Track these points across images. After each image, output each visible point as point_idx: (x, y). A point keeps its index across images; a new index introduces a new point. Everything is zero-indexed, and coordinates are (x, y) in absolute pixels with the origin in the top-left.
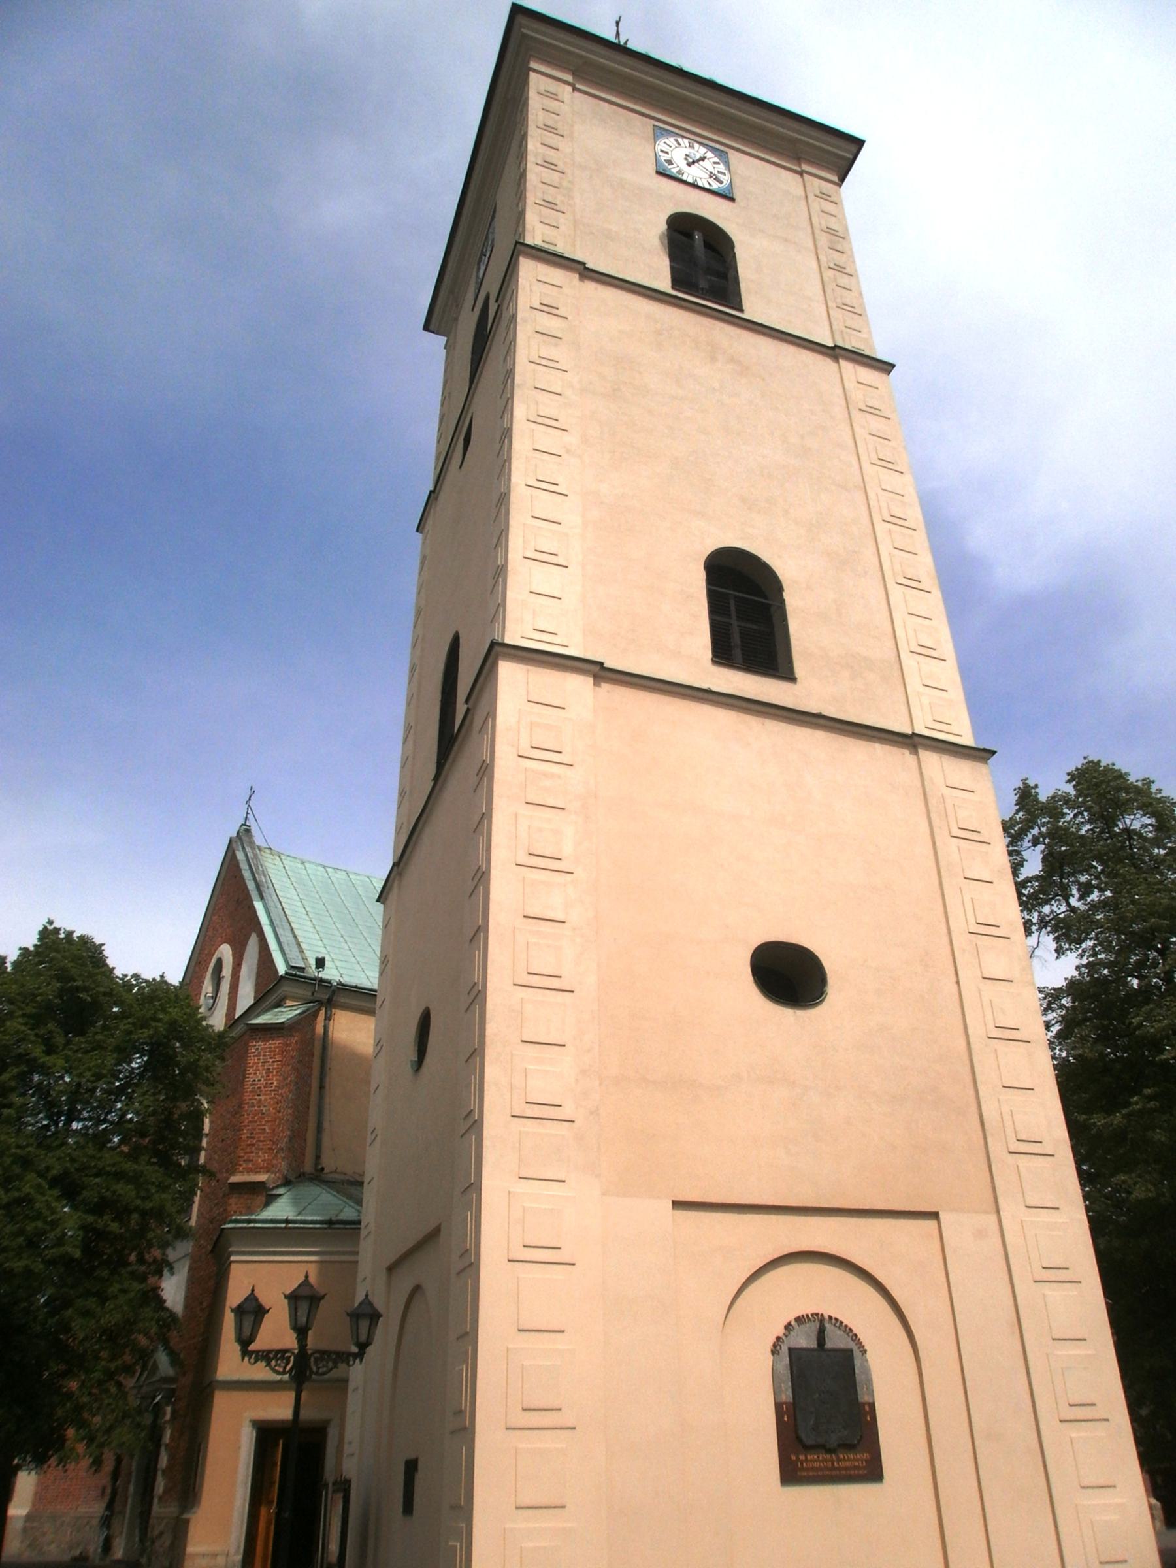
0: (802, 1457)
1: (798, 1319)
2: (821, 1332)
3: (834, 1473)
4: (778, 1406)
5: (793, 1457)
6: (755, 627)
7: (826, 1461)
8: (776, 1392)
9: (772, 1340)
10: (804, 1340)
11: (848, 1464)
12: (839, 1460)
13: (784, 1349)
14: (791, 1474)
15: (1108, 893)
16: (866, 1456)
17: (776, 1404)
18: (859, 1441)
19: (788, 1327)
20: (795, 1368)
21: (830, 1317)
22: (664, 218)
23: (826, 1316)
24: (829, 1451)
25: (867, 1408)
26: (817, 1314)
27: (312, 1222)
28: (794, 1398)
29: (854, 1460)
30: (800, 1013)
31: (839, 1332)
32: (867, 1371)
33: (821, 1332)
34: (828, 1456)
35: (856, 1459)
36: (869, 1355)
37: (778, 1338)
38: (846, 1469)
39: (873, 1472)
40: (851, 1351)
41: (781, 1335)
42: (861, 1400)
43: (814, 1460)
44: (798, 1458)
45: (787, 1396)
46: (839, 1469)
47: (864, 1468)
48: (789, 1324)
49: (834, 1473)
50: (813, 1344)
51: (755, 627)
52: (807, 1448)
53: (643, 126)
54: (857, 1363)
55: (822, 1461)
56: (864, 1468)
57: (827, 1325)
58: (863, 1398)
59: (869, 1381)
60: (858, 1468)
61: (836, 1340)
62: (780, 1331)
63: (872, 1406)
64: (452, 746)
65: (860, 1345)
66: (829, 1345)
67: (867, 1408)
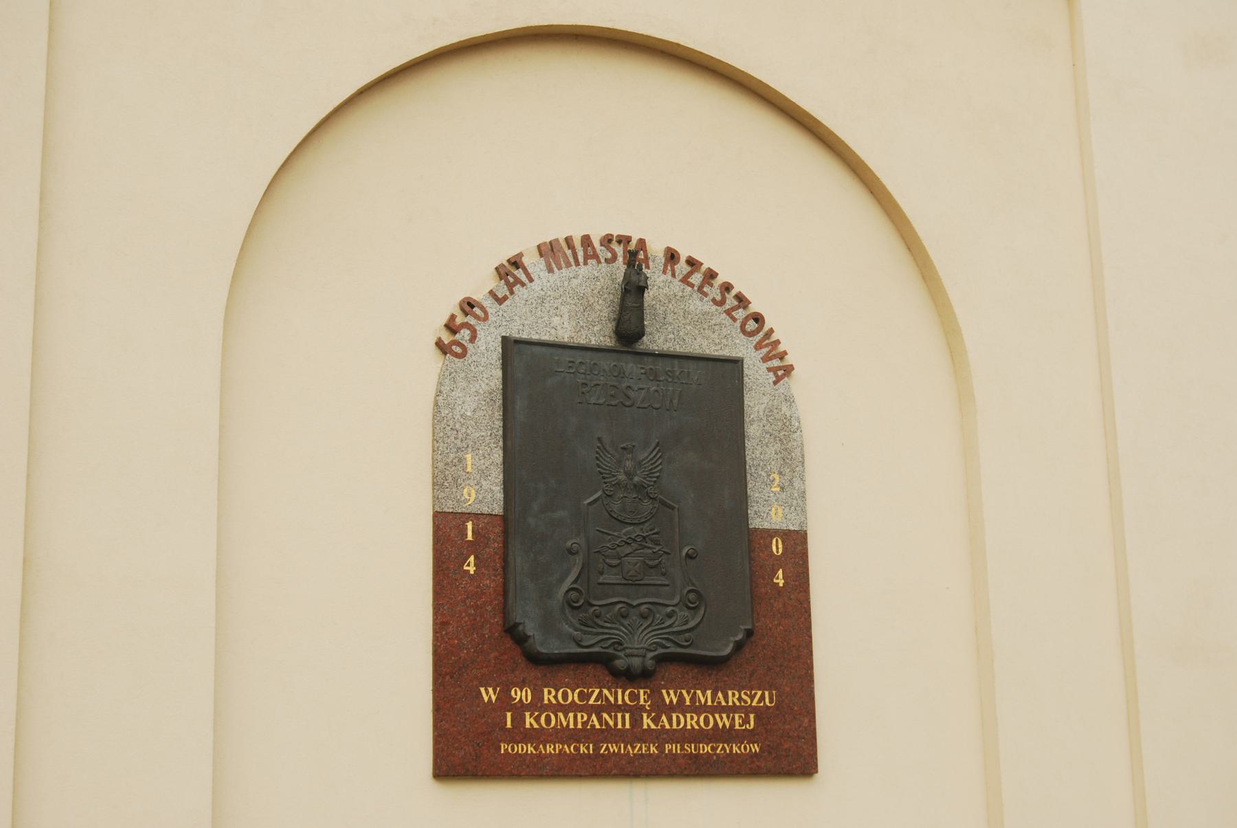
0: (521, 695)
1: (549, 251)
2: (633, 289)
3: (639, 748)
4: (446, 528)
5: (489, 694)
7: (612, 708)
9: (449, 307)
10: (567, 313)
11: (691, 721)
12: (660, 708)
13: (487, 348)
14: (468, 748)
15: (489, 694)
16: (762, 698)
17: (436, 515)
18: (739, 646)
19: (511, 271)
20: (520, 404)
21: (672, 256)
23: (656, 249)
24: (628, 677)
25: (777, 547)
26: (624, 240)
28: (506, 508)
29: (719, 709)
31: (698, 305)
32: (786, 430)
33: (633, 289)
35: (736, 705)
36: (797, 384)
37: (469, 305)
39: (784, 748)
40: (737, 363)
41: (480, 295)
43: (562, 705)
44: (505, 698)
45: (483, 492)
46: (660, 737)
47: (750, 736)
48: (516, 263)
49: (639, 748)
50: (599, 334)
52: (546, 665)
53: (613, 316)
54: (757, 401)
55: (598, 710)
56: (750, 736)
57: (656, 276)
58: (768, 512)
59: (792, 462)
60: (728, 735)
62: (481, 284)
63: (797, 542)
65: (772, 350)
66: (657, 339)
67: (777, 547)
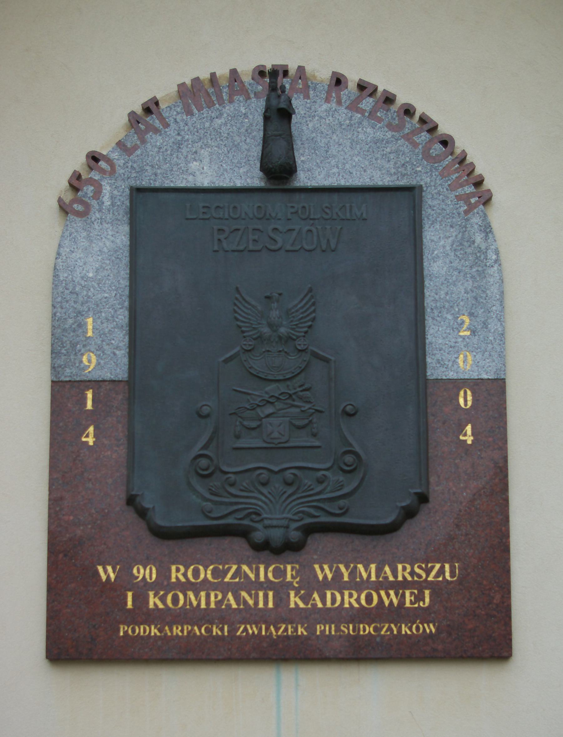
0: (145, 573)
2: (279, 116)
4: (65, 393)
7: (254, 586)
8: (64, 341)
12: (310, 584)
13: (113, 193)
25: (465, 399)
27: (302, 300)
30: (410, 102)
33: (279, 116)
34: (266, 573)
36: (496, 215)
41: (103, 147)
42: (435, 370)
43: (202, 583)
44: (125, 573)
45: (104, 358)
46: (310, 616)
47: (424, 615)
54: (437, 241)
55: (235, 589)
56: (424, 615)
61: (336, 154)
63: (492, 394)
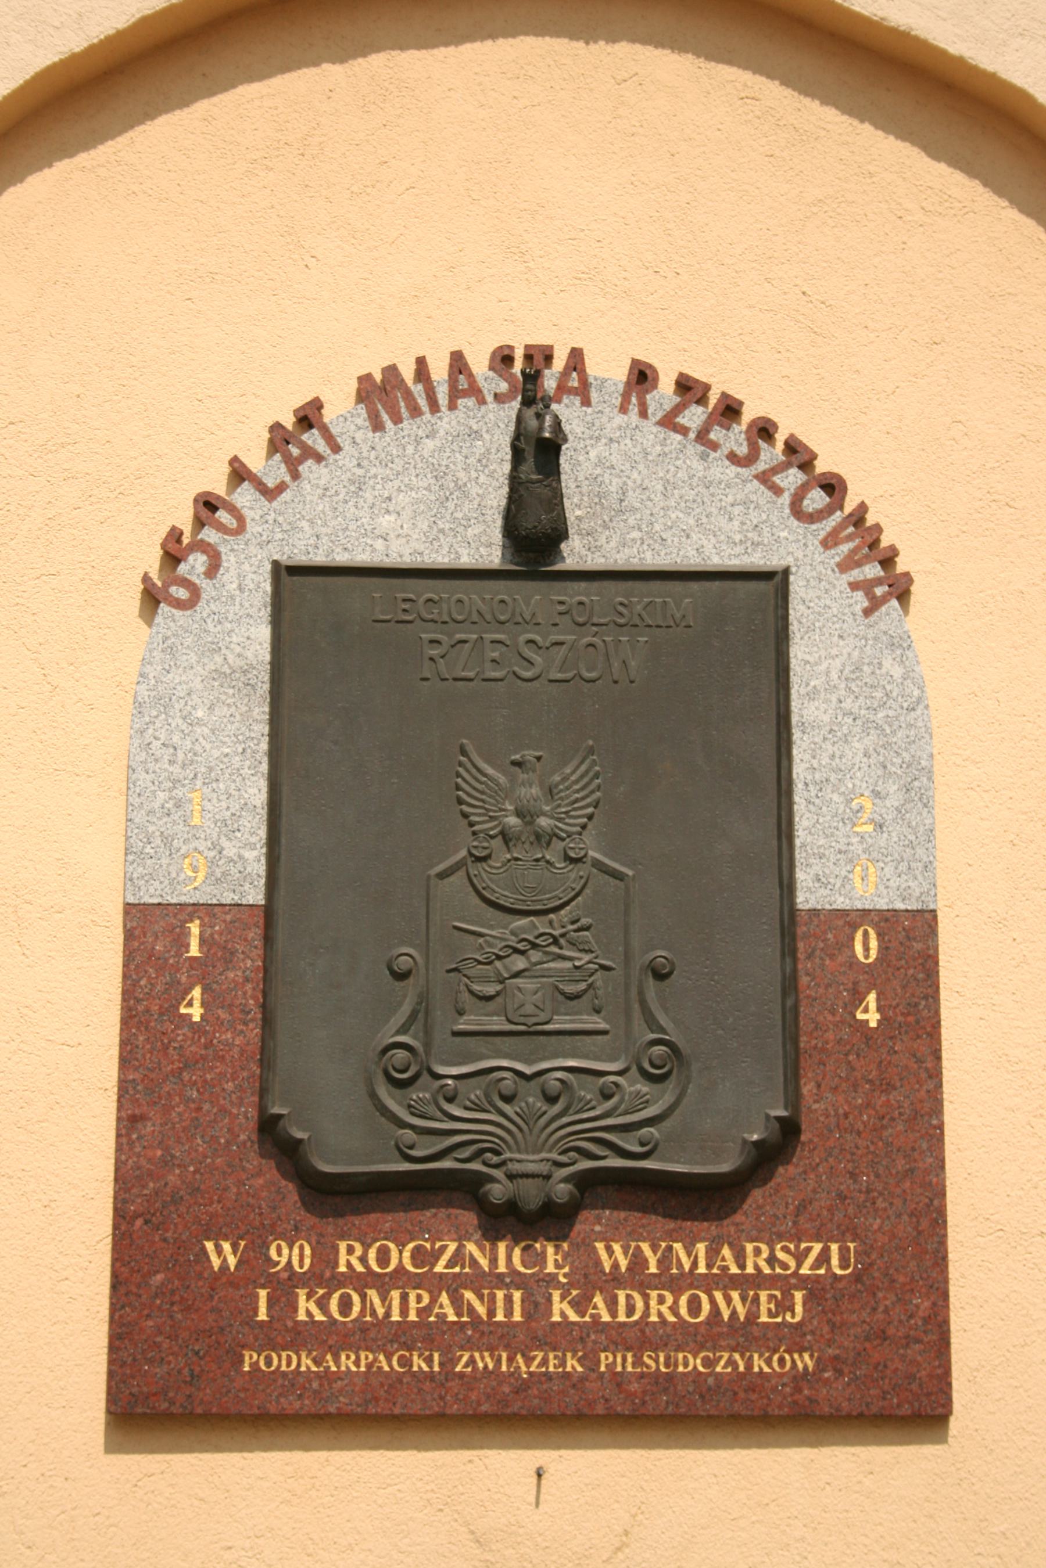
0: (290, 1255)
2: (538, 454)
6: (402, 404)
7: (484, 1281)
10: (425, 505)
11: (661, 1307)
12: (589, 1281)
16: (828, 1258)
22: (414, 360)
33: (538, 454)
34: (509, 1257)
35: (761, 1270)
38: (641, 1337)
40: (775, 582)
47: (795, 1338)
50: (483, 546)
51: (402, 404)
52: (337, 1197)
55: (453, 1286)
56: (795, 1338)
61: (646, 506)
64: (790, 803)
